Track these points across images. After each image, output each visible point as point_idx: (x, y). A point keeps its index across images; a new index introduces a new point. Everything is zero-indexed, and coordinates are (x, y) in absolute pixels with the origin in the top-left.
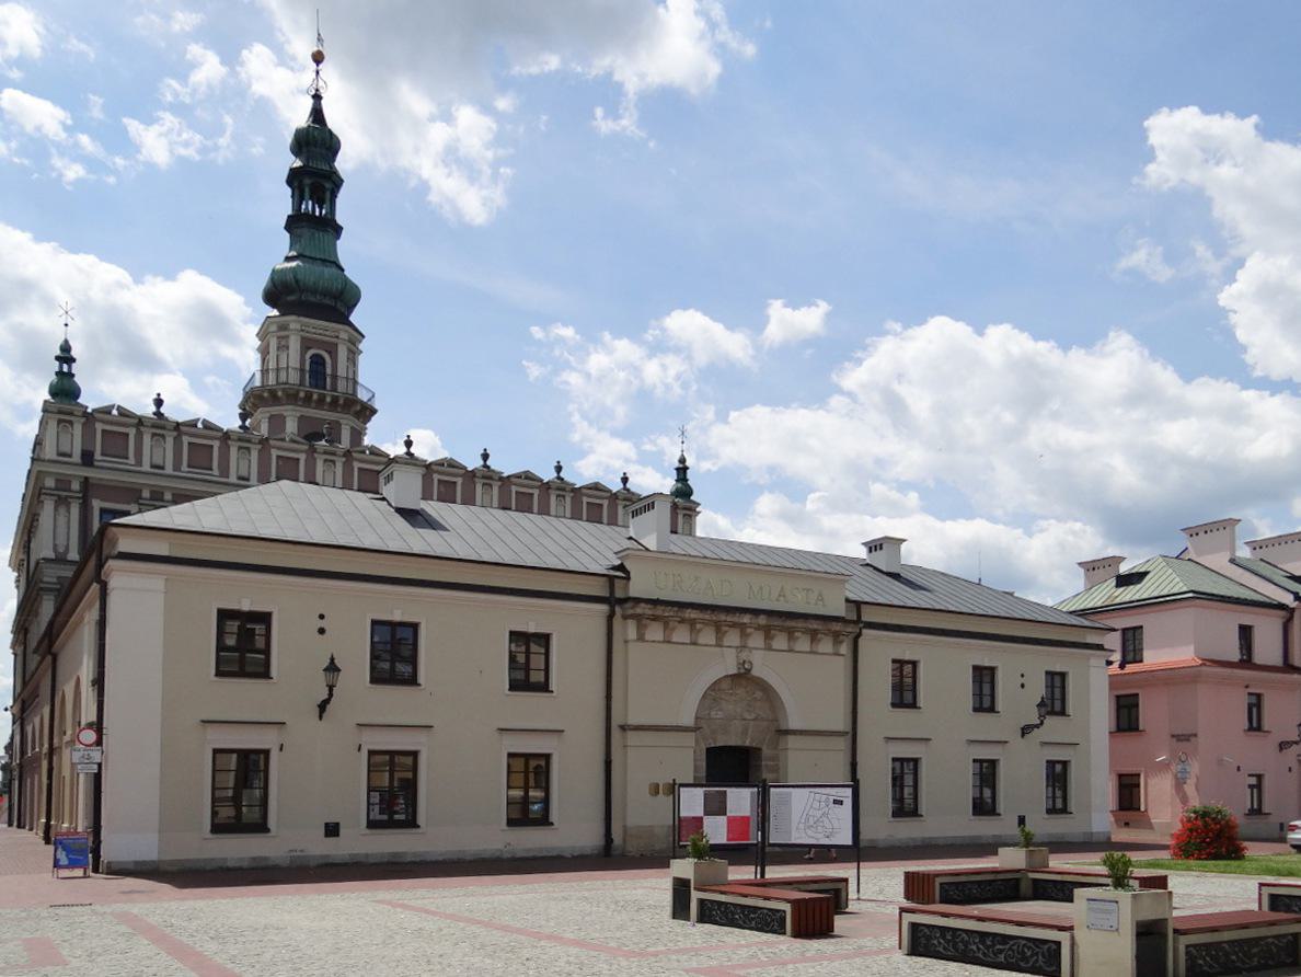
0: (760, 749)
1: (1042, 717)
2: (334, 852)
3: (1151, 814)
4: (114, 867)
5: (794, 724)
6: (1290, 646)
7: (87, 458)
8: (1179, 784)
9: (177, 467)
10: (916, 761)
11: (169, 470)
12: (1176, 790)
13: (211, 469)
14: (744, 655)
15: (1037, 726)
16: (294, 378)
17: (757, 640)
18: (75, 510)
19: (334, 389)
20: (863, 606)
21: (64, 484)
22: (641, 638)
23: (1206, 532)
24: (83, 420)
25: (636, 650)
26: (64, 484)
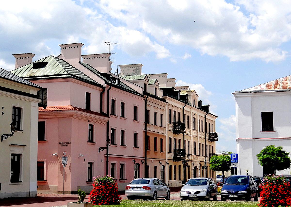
1: (13, 130)
3: (49, 182)
6: (103, 103)
8: (62, 167)
12: (61, 170)
15: (10, 135)
23: (69, 48)
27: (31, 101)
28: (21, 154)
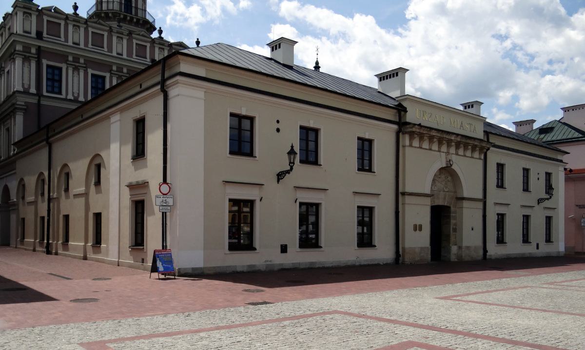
0: (449, 207)
2: (285, 262)
4: (182, 272)
5: (466, 195)
7: (39, 35)
9: (86, 44)
10: (317, 205)
11: (82, 46)
13: (103, 48)
14: (449, 157)
15: (288, 172)
16: (116, 7)
17: (453, 150)
18: (33, 65)
19: (136, 14)
20: (490, 135)
21: (27, 48)
22: (411, 145)
23: (573, 110)
24: (37, 13)
25: (408, 149)
26: (27, 48)
27: (559, 166)
28: (530, 215)
